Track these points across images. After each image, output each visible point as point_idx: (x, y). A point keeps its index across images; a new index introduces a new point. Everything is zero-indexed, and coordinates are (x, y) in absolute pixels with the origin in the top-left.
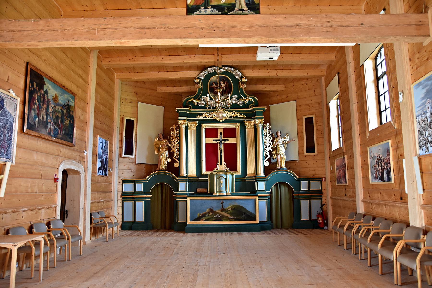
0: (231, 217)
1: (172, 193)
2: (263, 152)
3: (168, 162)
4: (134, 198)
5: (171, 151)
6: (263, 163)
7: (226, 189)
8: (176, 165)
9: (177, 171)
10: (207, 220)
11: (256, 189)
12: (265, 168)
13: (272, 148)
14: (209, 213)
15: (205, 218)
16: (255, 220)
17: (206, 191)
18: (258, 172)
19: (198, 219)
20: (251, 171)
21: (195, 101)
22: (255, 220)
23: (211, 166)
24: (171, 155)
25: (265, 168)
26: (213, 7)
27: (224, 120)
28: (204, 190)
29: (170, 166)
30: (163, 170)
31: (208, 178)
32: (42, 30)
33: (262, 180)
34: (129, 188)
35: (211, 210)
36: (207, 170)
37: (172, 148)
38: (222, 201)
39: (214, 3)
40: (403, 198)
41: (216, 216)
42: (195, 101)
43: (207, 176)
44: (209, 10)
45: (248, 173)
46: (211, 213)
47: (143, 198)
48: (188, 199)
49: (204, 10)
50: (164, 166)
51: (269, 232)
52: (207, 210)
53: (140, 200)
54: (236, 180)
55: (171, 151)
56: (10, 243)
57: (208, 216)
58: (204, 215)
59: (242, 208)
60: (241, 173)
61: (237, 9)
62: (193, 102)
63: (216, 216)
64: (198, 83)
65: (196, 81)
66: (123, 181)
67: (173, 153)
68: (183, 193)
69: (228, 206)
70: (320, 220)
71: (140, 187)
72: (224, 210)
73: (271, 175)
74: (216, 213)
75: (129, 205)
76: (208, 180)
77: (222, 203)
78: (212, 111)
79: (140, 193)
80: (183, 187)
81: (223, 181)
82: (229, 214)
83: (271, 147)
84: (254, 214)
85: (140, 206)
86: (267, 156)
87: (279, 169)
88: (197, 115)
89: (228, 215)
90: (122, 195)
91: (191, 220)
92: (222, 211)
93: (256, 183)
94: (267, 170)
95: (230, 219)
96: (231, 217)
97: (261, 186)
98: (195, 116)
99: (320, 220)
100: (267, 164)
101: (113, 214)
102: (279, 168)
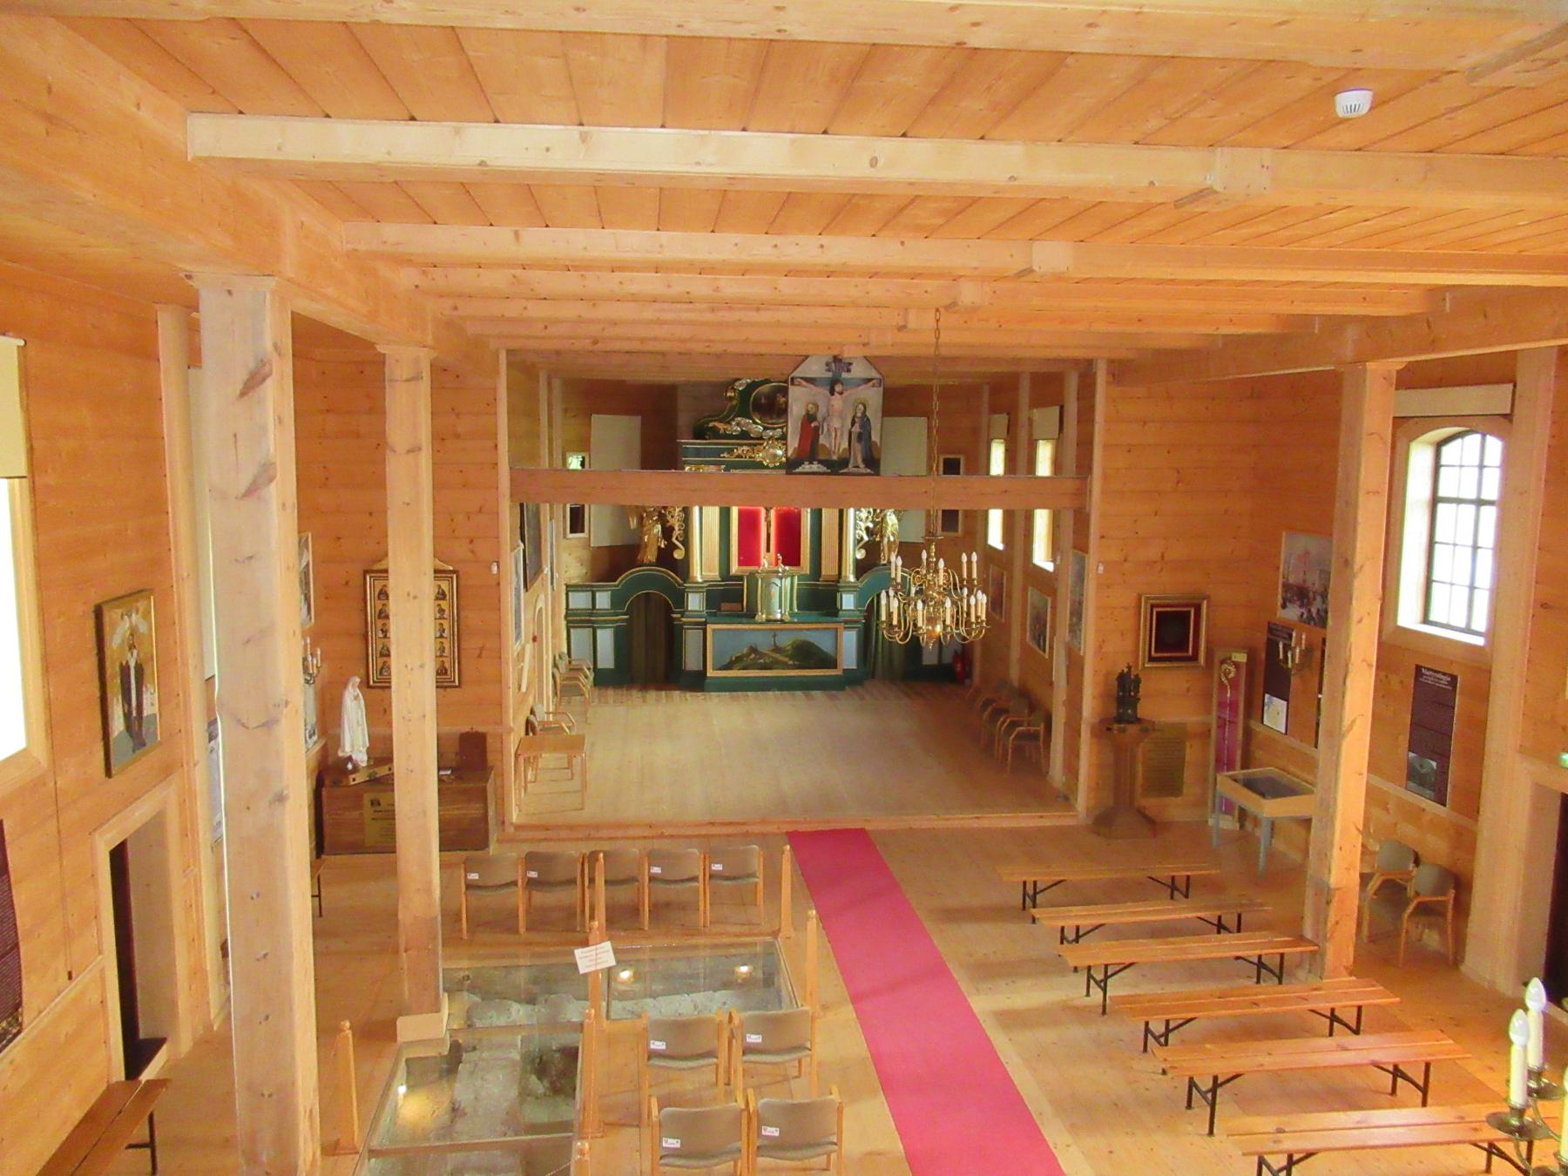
0: (791, 662)
1: (669, 611)
2: (855, 529)
3: (659, 547)
5: (668, 525)
6: (854, 553)
7: (780, 607)
8: (678, 555)
9: (683, 568)
13: (873, 521)
14: (748, 655)
15: (741, 665)
16: (836, 667)
17: (740, 608)
18: (843, 574)
19: (728, 667)
20: (828, 569)
21: (721, 426)
22: (836, 667)
23: (749, 555)
25: (858, 563)
28: (735, 606)
29: (665, 557)
33: (850, 588)
34: (580, 601)
35: (753, 650)
37: (669, 518)
38: (775, 633)
40: (457, 1085)
41: (762, 661)
43: (740, 578)
45: (823, 573)
46: (753, 656)
47: (611, 621)
50: (651, 556)
51: (859, 689)
53: (603, 626)
54: (798, 585)
57: (747, 661)
58: (739, 659)
63: (762, 661)
65: (729, 394)
66: (567, 586)
67: (672, 529)
68: (697, 614)
69: (786, 641)
70: (959, 667)
71: (603, 600)
72: (777, 649)
74: (762, 655)
75: (581, 636)
76: (743, 585)
77: (774, 636)
79: (604, 613)
80: (695, 602)
81: (775, 591)
82: (786, 656)
83: (870, 519)
85: (606, 638)
86: (862, 539)
88: (723, 451)
89: (786, 659)
90: (566, 616)
91: (715, 668)
92: (774, 651)
93: (838, 595)
94: (861, 568)
95: (786, 666)
96: (791, 662)
97: (848, 602)
99: (959, 667)
100: (861, 555)
101: (21, 484)
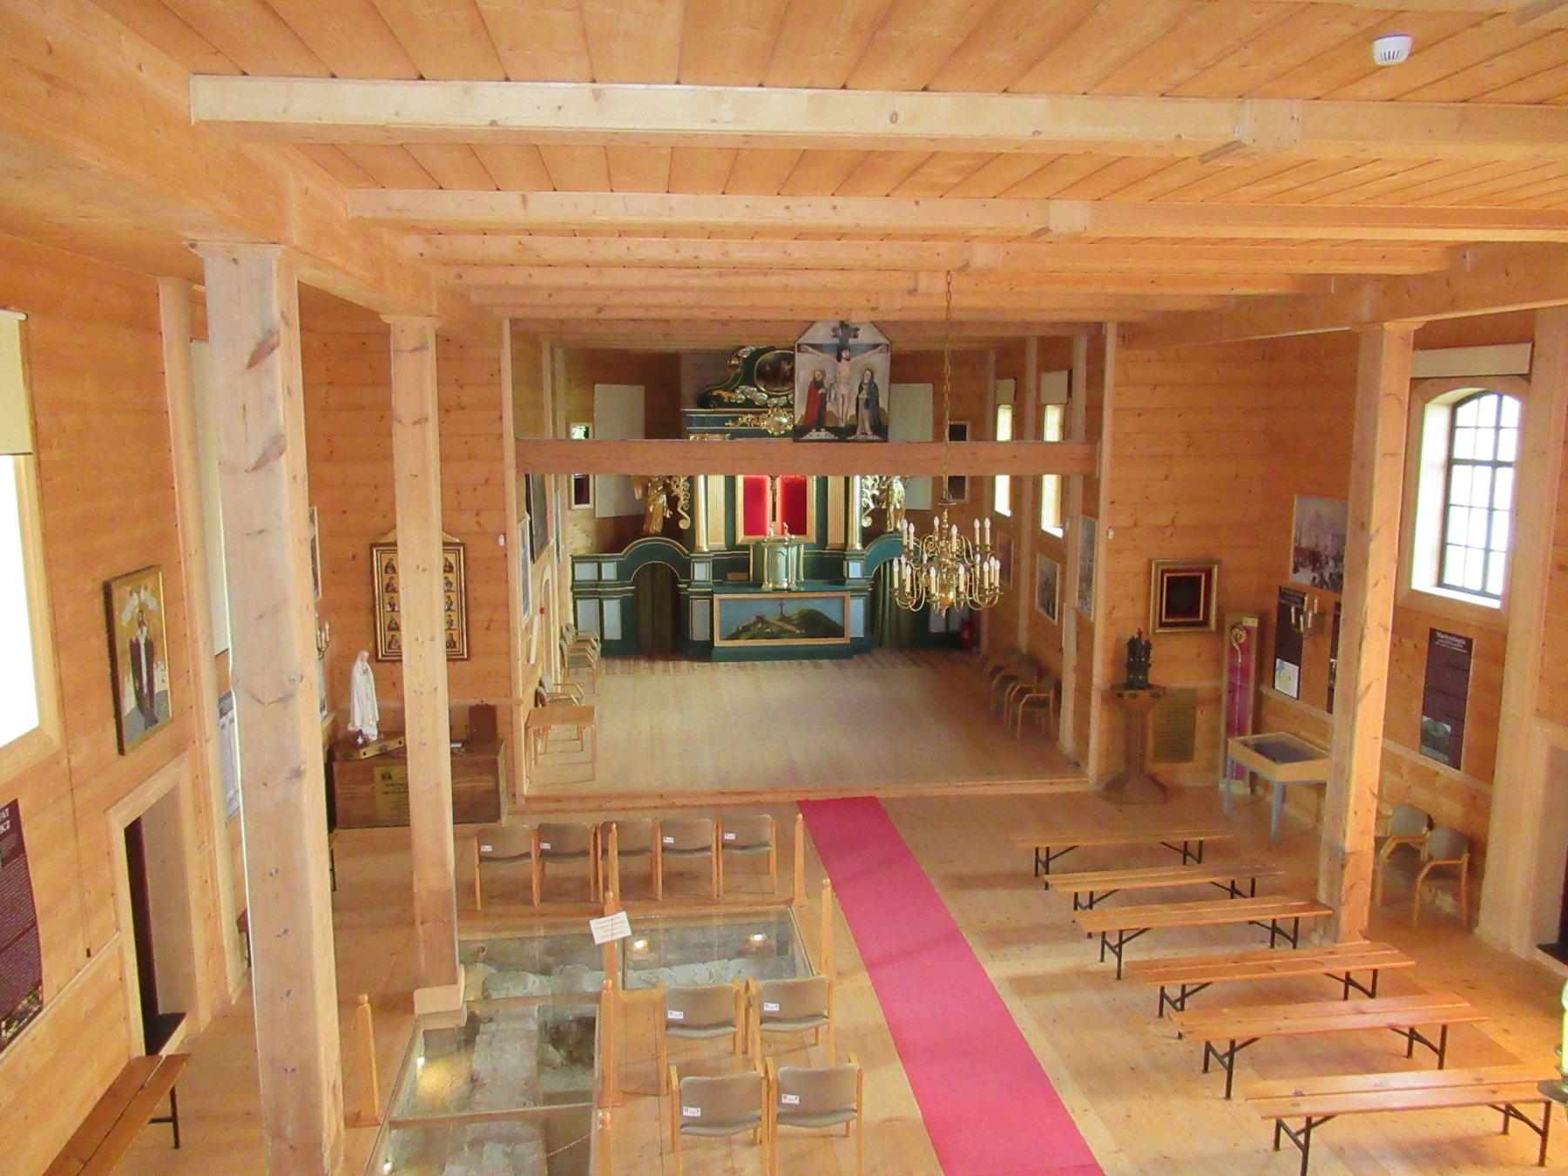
0: (798, 632)
1: (675, 581)
2: (861, 497)
3: (665, 518)
4: (600, 593)
5: (673, 494)
6: (860, 522)
8: (684, 525)
9: (689, 538)
10: (753, 637)
11: (845, 574)
12: (864, 531)
14: (755, 623)
15: (749, 634)
19: (735, 637)
20: (834, 537)
21: (725, 394)
24: (673, 502)
25: (864, 531)
26: (828, 429)
27: (783, 432)
30: (656, 534)
31: (749, 550)
32: (600, 457)
33: (857, 556)
34: (586, 572)
35: (760, 619)
36: (747, 532)
37: (674, 488)
38: (781, 602)
39: (829, 425)
41: (769, 630)
42: (725, 394)
43: (746, 547)
44: (823, 434)
46: (760, 625)
48: (716, 597)
49: (816, 434)
52: (753, 619)
54: (805, 554)
55: (673, 494)
56: (1038, 791)
57: (755, 630)
58: (746, 629)
59: (819, 613)
60: (815, 541)
61: (858, 433)
62: (719, 395)
63: (769, 630)
64: (735, 366)
65: (733, 362)
68: (702, 584)
69: (792, 610)
70: (966, 635)
71: (609, 571)
72: (784, 618)
73: (873, 547)
74: (769, 624)
75: (587, 607)
76: (749, 554)
77: (782, 605)
78: (760, 413)
80: (701, 572)
81: (781, 560)
82: (793, 625)
83: (876, 486)
84: (838, 621)
85: (612, 609)
86: (868, 506)
87: (891, 533)
88: (727, 420)
92: (779, 620)
93: (845, 563)
94: (868, 536)
95: (793, 635)
96: (798, 632)
97: (854, 570)
98: (721, 421)
100: (867, 523)
102: (892, 530)
